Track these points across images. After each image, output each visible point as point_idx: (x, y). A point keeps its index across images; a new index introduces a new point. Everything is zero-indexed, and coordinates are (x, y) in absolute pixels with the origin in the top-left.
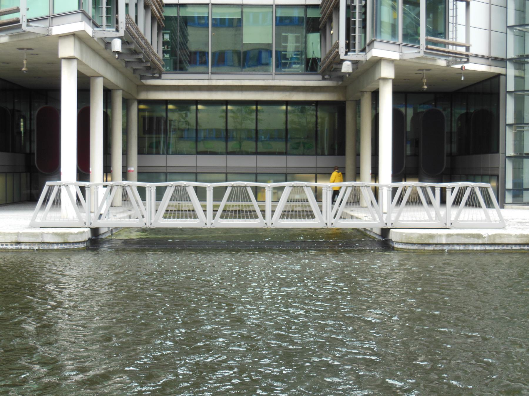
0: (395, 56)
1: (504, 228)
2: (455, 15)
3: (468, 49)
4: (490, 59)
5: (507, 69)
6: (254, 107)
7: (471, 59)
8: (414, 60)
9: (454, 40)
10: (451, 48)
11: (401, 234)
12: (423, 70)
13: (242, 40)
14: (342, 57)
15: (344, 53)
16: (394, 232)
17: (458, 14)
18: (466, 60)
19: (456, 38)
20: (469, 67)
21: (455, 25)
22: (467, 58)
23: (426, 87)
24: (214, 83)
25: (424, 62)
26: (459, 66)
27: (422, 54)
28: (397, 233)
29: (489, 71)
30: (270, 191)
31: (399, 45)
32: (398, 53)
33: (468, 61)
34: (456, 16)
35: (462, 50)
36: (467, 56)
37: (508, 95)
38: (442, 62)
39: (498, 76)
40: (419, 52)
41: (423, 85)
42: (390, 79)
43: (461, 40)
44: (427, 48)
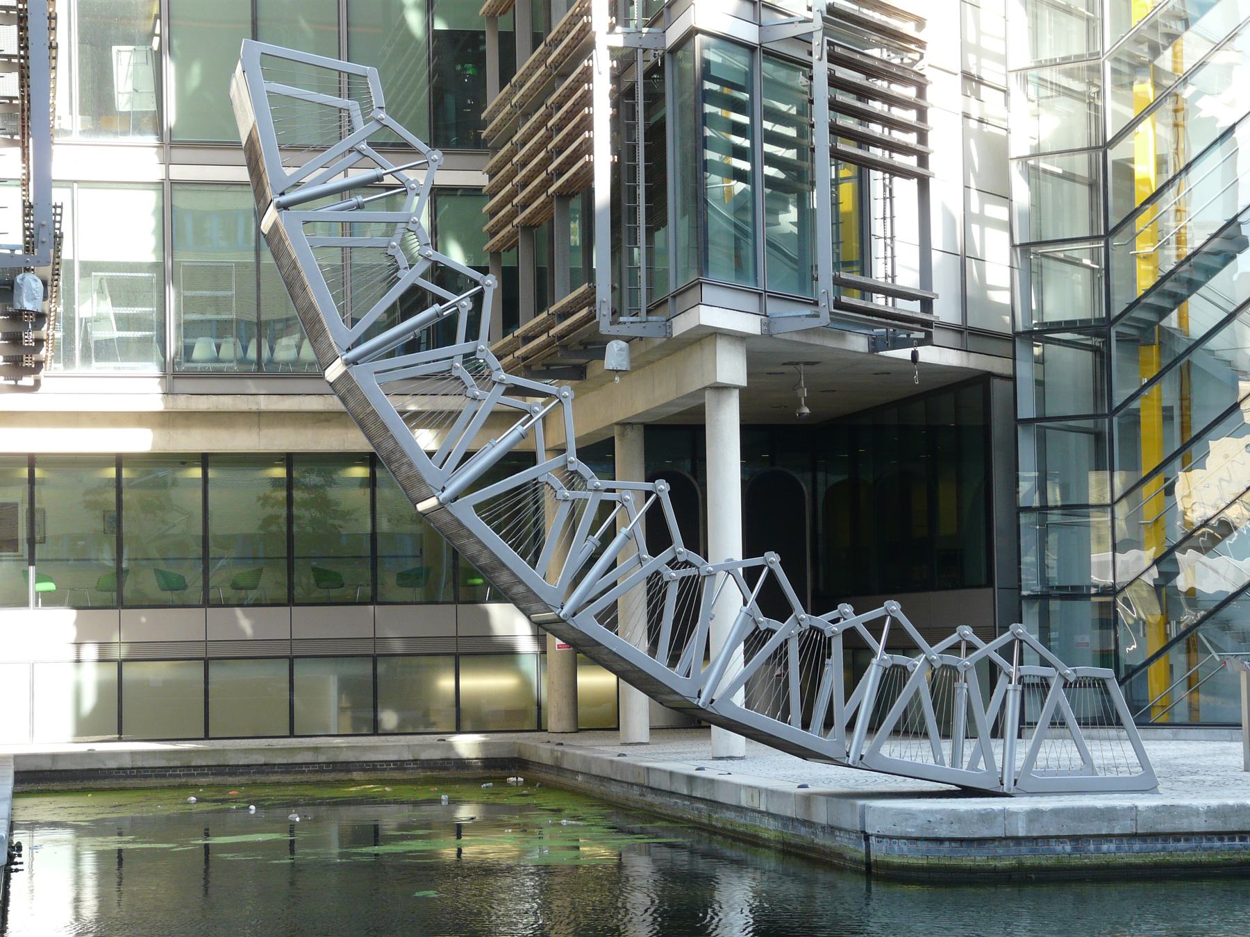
0: (750, 324)
1: (1152, 789)
2: (888, 215)
3: (927, 304)
4: (966, 333)
5: (1018, 362)
6: (197, 473)
7: (937, 335)
8: (796, 338)
9: (890, 280)
10: (879, 301)
11: (910, 814)
12: (798, 363)
13: (976, 214)
14: (605, 327)
15: (609, 318)
16: (875, 809)
17: (896, 213)
18: (922, 335)
19: (893, 277)
20: (928, 355)
21: (888, 241)
22: (926, 329)
23: (806, 410)
24: (265, 404)
25: (816, 340)
26: (905, 354)
27: (825, 319)
28: (885, 810)
29: (965, 365)
30: (912, 742)
31: (760, 295)
32: (759, 318)
33: (927, 341)
34: (892, 217)
35: (913, 308)
36: (928, 324)
37: (1020, 429)
38: (858, 343)
39: (983, 379)
40: (816, 316)
41: (800, 406)
42: (735, 387)
43: (908, 279)
44: (838, 305)
